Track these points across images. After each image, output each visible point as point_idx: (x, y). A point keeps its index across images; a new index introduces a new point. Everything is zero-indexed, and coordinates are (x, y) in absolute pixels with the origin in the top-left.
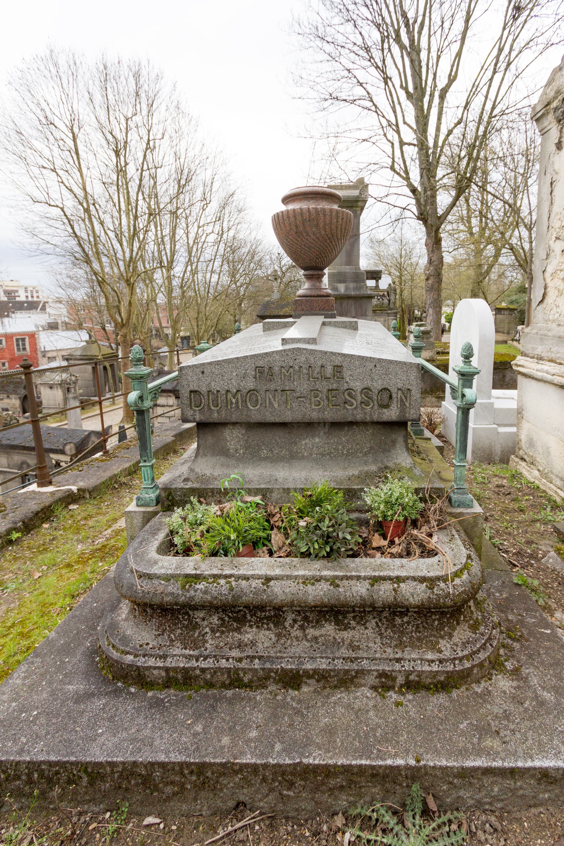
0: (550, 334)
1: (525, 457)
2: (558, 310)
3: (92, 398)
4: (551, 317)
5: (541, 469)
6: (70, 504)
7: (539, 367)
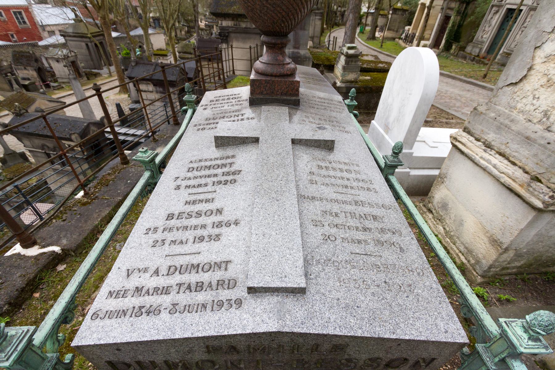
0: (513, 128)
1: (434, 211)
2: (535, 102)
3: (93, 71)
4: (519, 106)
5: (448, 229)
6: (57, 265)
7: (486, 156)
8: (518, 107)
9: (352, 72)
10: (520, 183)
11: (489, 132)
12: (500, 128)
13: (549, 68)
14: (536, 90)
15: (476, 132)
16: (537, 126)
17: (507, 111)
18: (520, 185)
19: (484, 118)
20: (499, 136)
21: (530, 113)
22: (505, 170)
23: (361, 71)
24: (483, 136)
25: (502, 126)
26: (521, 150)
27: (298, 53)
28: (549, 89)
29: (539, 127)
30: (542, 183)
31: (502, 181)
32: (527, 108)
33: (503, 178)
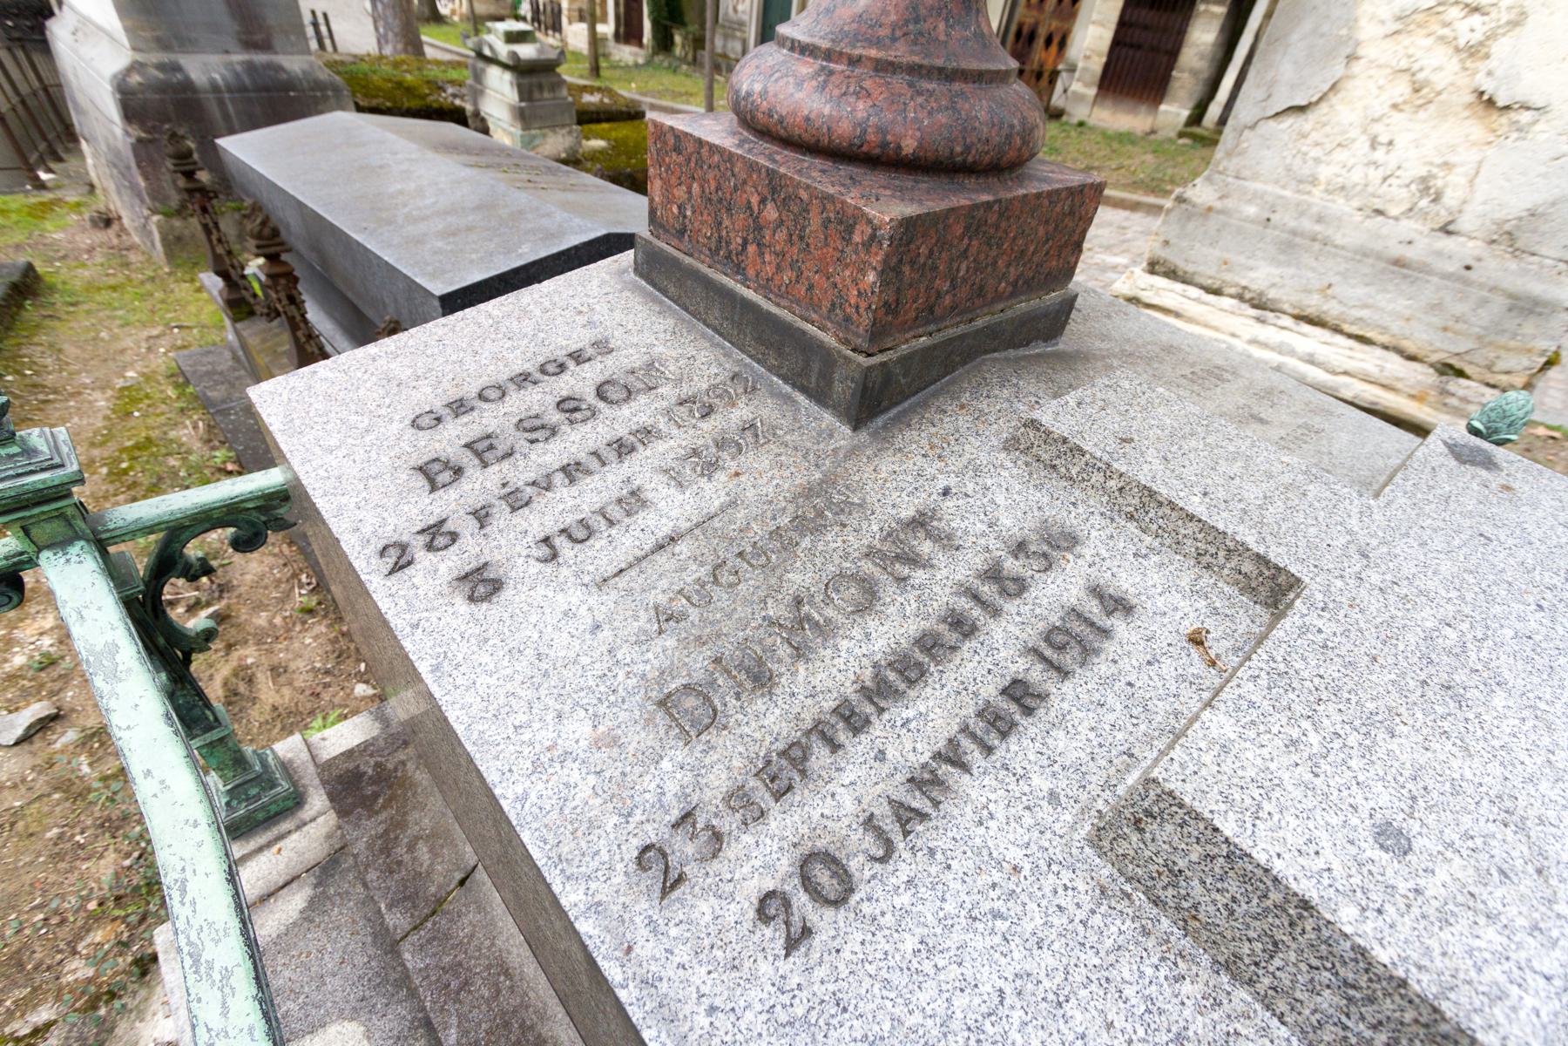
0: (1339, 239)
4: (1325, 172)
7: (1268, 333)
8: (1322, 178)
9: (553, 127)
10: (1413, 392)
11: (1251, 263)
12: (1291, 245)
13: (1411, 51)
14: (1375, 120)
15: (1201, 269)
16: (1404, 223)
17: (1287, 193)
18: (1412, 397)
19: (1224, 225)
20: (1292, 271)
21: (1370, 189)
22: (1351, 365)
23: (580, 123)
24: (1228, 277)
25: (1298, 240)
26: (1382, 300)
27: (280, 68)
28: (1422, 115)
29: (1409, 227)
30: (1468, 377)
31: (1348, 395)
32: (1356, 176)
33: (1347, 386)
